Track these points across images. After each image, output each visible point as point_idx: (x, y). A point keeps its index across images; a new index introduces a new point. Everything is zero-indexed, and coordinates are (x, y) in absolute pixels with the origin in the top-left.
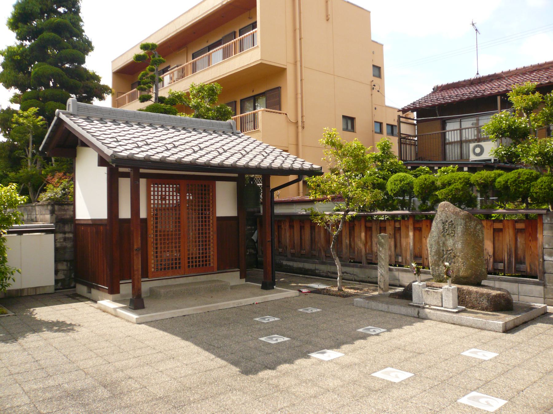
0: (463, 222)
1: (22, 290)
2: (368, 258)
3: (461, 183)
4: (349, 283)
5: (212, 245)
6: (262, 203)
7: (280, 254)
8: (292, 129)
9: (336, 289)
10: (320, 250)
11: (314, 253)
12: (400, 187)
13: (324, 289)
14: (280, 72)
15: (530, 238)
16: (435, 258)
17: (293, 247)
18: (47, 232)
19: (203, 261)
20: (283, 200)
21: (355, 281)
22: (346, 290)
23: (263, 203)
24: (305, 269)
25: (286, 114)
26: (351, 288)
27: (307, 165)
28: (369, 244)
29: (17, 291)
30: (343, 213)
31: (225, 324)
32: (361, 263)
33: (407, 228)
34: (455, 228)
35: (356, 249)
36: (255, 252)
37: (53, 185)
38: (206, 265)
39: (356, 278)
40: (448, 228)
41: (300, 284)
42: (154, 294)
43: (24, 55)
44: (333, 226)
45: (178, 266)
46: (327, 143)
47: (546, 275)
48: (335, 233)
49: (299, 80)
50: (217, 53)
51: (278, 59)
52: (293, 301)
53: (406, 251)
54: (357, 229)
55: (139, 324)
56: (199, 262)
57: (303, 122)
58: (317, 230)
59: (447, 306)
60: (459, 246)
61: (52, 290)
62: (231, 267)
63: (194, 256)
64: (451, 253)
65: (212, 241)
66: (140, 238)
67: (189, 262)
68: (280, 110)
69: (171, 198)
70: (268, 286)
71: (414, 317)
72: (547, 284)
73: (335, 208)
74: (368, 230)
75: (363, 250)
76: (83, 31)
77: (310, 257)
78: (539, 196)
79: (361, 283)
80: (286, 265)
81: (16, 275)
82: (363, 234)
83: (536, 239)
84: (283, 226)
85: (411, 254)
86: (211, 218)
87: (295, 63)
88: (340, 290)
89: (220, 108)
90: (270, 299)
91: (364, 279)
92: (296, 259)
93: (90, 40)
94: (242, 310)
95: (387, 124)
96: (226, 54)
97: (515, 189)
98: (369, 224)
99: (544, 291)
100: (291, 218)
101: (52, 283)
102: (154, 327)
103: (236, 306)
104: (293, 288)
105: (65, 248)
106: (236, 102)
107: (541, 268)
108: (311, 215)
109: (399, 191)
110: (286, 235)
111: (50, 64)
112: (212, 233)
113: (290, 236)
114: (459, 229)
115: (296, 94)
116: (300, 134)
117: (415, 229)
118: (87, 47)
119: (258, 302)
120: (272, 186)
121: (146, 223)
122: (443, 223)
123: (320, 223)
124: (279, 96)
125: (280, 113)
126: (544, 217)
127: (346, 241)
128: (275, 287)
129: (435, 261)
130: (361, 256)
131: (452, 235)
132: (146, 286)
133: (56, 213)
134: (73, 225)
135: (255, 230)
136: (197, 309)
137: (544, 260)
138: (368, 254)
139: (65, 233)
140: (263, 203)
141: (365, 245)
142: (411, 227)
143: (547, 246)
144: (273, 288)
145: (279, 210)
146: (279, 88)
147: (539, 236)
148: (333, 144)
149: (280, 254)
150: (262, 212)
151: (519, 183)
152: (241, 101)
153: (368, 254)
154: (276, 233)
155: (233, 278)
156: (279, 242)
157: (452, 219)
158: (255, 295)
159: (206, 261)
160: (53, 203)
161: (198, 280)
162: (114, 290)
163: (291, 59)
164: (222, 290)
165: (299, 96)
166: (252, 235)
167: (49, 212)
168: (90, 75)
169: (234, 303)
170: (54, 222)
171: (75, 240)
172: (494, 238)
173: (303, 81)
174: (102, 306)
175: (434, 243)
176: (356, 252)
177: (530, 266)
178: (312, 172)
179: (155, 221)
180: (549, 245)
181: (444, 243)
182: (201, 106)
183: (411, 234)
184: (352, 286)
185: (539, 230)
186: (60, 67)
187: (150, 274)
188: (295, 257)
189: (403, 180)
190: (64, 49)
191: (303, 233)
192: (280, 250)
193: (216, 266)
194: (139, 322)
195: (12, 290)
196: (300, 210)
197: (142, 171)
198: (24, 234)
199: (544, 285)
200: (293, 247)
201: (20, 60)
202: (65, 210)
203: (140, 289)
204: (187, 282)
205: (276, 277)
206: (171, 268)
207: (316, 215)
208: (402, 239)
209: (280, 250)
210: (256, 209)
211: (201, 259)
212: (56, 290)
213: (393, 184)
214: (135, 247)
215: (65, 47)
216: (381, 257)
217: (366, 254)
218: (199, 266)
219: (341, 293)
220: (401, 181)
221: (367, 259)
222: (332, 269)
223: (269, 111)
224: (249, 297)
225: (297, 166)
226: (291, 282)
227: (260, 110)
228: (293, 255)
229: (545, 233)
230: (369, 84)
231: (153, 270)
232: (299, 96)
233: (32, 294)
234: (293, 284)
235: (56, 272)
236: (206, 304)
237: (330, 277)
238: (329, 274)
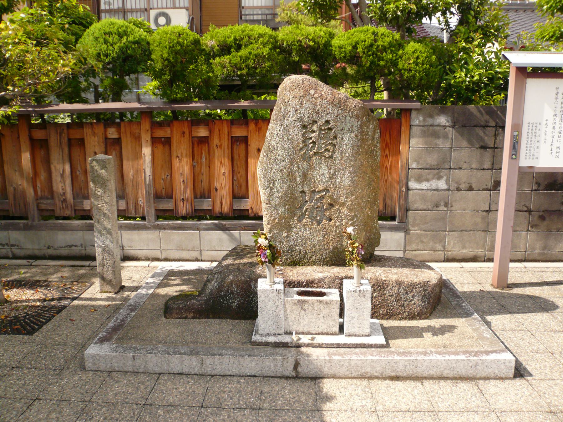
0: (356, 123)
2: (43, 207)
3: (264, 44)
12: (121, 49)
15: (387, 152)
16: (281, 210)
21: (15, 257)
26: (18, 284)
28: (43, 176)
30: (179, 57)
32: (26, 218)
33: (137, 139)
34: (335, 138)
35: (10, 189)
39: (17, 251)
40: (316, 137)
47: (410, 213)
53: (136, 186)
59: (355, 331)
60: (345, 180)
64: (322, 197)
71: (287, 378)
72: (411, 228)
74: (39, 146)
75: (30, 192)
78: (414, 76)
82: (26, 157)
83: (397, 152)
85: (148, 193)
91: (37, 253)
97: (372, 62)
99: (405, 239)
107: (402, 202)
109: (118, 57)
114: (347, 141)
117: (155, 141)
122: (304, 127)
126: (414, 114)
129: (281, 217)
130: (26, 204)
131: (327, 154)
137: (408, 189)
138: (42, 198)
142: (146, 137)
143: (414, 165)
147: (403, 148)
151: (378, 51)
153: (42, 198)
157: (328, 118)
172: (193, 151)
175: (278, 176)
176: (11, 197)
177: (384, 200)
180: (418, 163)
181: (305, 176)
183: (147, 151)
184: (15, 277)
185: (404, 137)
189: (126, 33)
199: (406, 231)
208: (125, 162)
213: (102, 40)
216: (100, 210)
217: (37, 198)
220: (120, 36)
221: (40, 210)
229: (413, 142)
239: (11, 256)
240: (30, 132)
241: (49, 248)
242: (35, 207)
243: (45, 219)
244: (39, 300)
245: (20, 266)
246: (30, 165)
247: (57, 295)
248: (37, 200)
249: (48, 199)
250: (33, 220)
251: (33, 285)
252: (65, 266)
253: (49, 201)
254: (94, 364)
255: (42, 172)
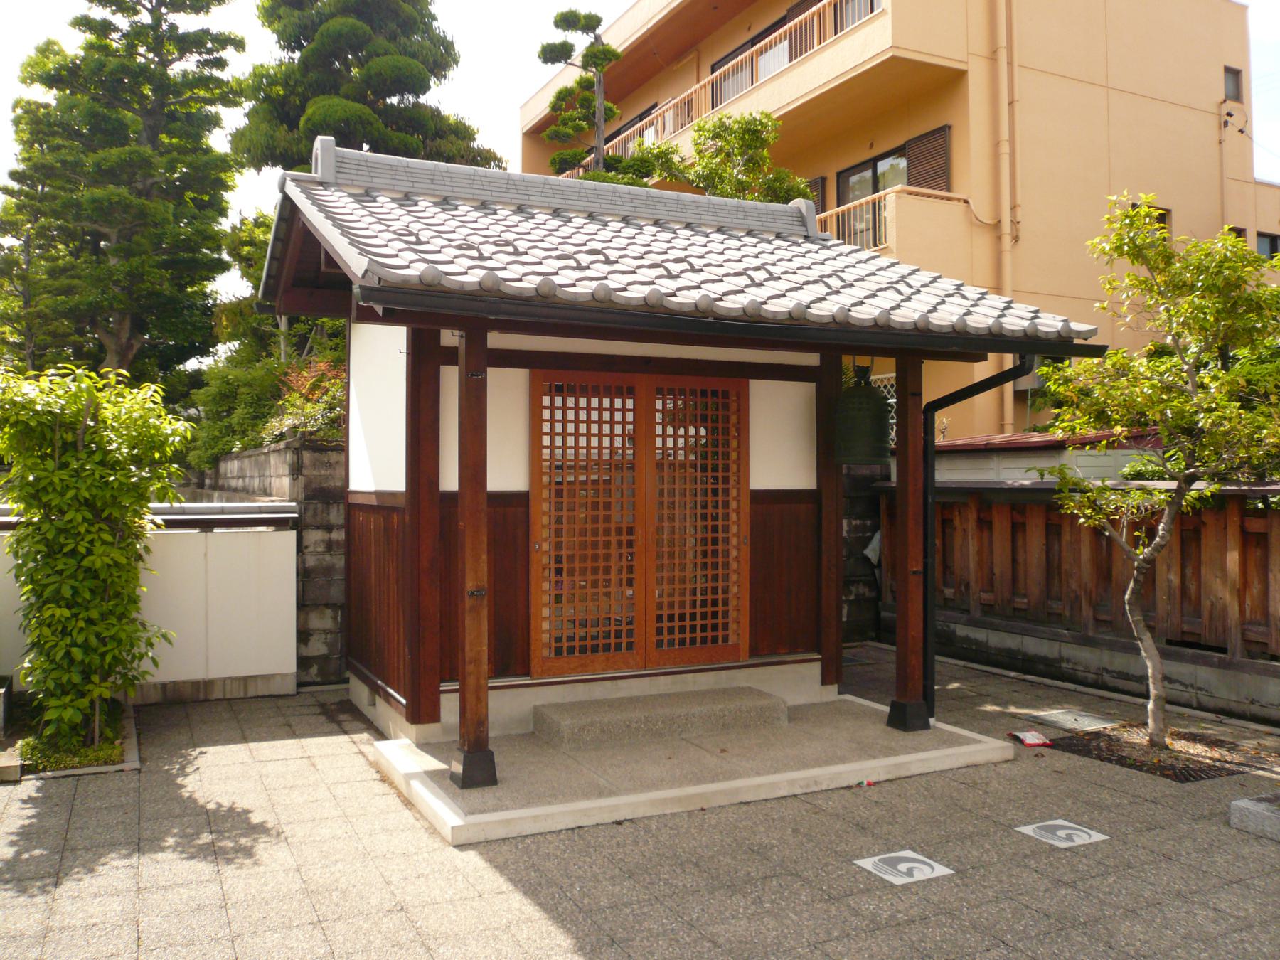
1: (208, 684)
2: (1252, 636)
4: (1181, 716)
5: (734, 577)
6: (893, 453)
7: (947, 603)
8: (983, 243)
9: (1139, 737)
10: (1077, 598)
11: (1056, 606)
13: (1097, 735)
14: (948, 81)
17: (990, 585)
18: (280, 524)
19: (704, 628)
20: (959, 442)
21: (1201, 707)
22: (1179, 745)
23: (899, 452)
24: (1025, 654)
25: (966, 202)
26: (1193, 738)
27: (1050, 323)
28: (1256, 588)
29: (196, 684)
30: (1173, 485)
31: (749, 880)
32: (1224, 651)
35: (1206, 604)
36: (873, 594)
37: (302, 395)
38: (715, 640)
39: (1205, 700)
41: (1013, 709)
42: (539, 732)
43: (292, 83)
44: (1134, 526)
45: (624, 641)
46: (1118, 248)
48: (1143, 552)
49: (1004, 103)
50: (775, 57)
51: (940, 46)
52: (995, 784)
54: (1209, 540)
55: (461, 847)
56: (693, 629)
57: (1015, 223)
58: (1066, 537)
61: (290, 687)
62: (793, 649)
63: (677, 611)
65: (734, 565)
66: (484, 557)
67: (660, 631)
68: (949, 190)
69: (606, 429)
70: (909, 715)
73: (1126, 470)
76: (434, 18)
77: (1038, 618)
79: (1226, 720)
80: (967, 639)
81: (160, 648)
82: (1233, 558)
84: (957, 522)
86: (734, 493)
87: (993, 57)
88: (1155, 744)
89: (775, 180)
90: (915, 770)
91: (1234, 706)
92: (997, 621)
93: (449, 38)
94: (817, 810)
95: (1260, 235)
96: (798, 48)
98: (1255, 525)
100: (985, 500)
101: (291, 667)
102: (501, 868)
103: (798, 791)
104: (987, 725)
105: (328, 570)
106: (824, 180)
108: (1060, 491)
110: (968, 548)
111: (347, 97)
112: (734, 541)
113: (980, 552)
115: (996, 145)
116: (1007, 259)
118: (440, 58)
119: (873, 779)
120: (928, 396)
121: (527, 506)
123: (1088, 517)
124: (944, 154)
125: (949, 199)
127: (1169, 577)
128: (932, 721)
132: (508, 704)
133: (305, 472)
134: (342, 506)
135: (875, 529)
136: (664, 801)
138: (1251, 623)
139: (329, 528)
140: (899, 452)
141: (1241, 593)
144: (926, 726)
145: (948, 474)
146: (945, 130)
148: (1138, 253)
149: (947, 603)
150: (894, 477)
152: (839, 174)
153: (1251, 623)
154: (938, 542)
155: (799, 682)
156: (946, 567)
158: (866, 751)
159: (715, 628)
160: (297, 445)
161: (691, 688)
162: (421, 711)
163: (981, 46)
164: (756, 724)
165: (1005, 148)
166: (865, 546)
167: (286, 470)
168: (450, 125)
169: (792, 783)
170: (301, 496)
171: (349, 547)
173: (1017, 106)
174: (383, 761)
176: (1206, 614)
178: (1061, 347)
179: (553, 500)
182: (721, 177)
184: (1193, 730)
186: (372, 105)
187: (535, 665)
188: (991, 614)
190: (378, 55)
191: (1020, 543)
192: (949, 592)
193: (745, 646)
194: (462, 840)
195: (184, 682)
196: (1018, 474)
197: (496, 340)
198: (217, 530)
200: (990, 585)
201: (285, 97)
202: (329, 465)
203: (482, 723)
204: (654, 692)
205: (937, 677)
206: (597, 648)
207: (1078, 488)
209: (949, 592)
210: (877, 469)
211: (699, 622)
212: (300, 684)
214: (470, 585)
215: (381, 51)
217: (1243, 622)
218: (692, 638)
219: (1163, 755)
221: (1247, 642)
222: (1119, 661)
223: (917, 194)
224: (842, 760)
225: (1016, 321)
226: (985, 698)
227: (893, 197)
228: (988, 608)
230: (1215, 111)
231: (545, 652)
232: (1005, 148)
233: (235, 695)
234: (989, 708)
235: (303, 636)
236: (699, 781)
237: (1117, 690)
238: (1107, 678)
239: (1195, 704)
240: (1242, 522)
241: (1252, 702)
242: (1239, 636)
243: (1252, 656)
244: (1210, 758)
245: (1203, 720)
246: (1237, 569)
247: (1242, 760)
248: (1243, 624)
249: (1260, 625)
250: (1234, 654)
251: (1212, 743)
252: (1272, 734)
253: (1261, 629)
254: (1242, 821)
255: (1256, 582)
